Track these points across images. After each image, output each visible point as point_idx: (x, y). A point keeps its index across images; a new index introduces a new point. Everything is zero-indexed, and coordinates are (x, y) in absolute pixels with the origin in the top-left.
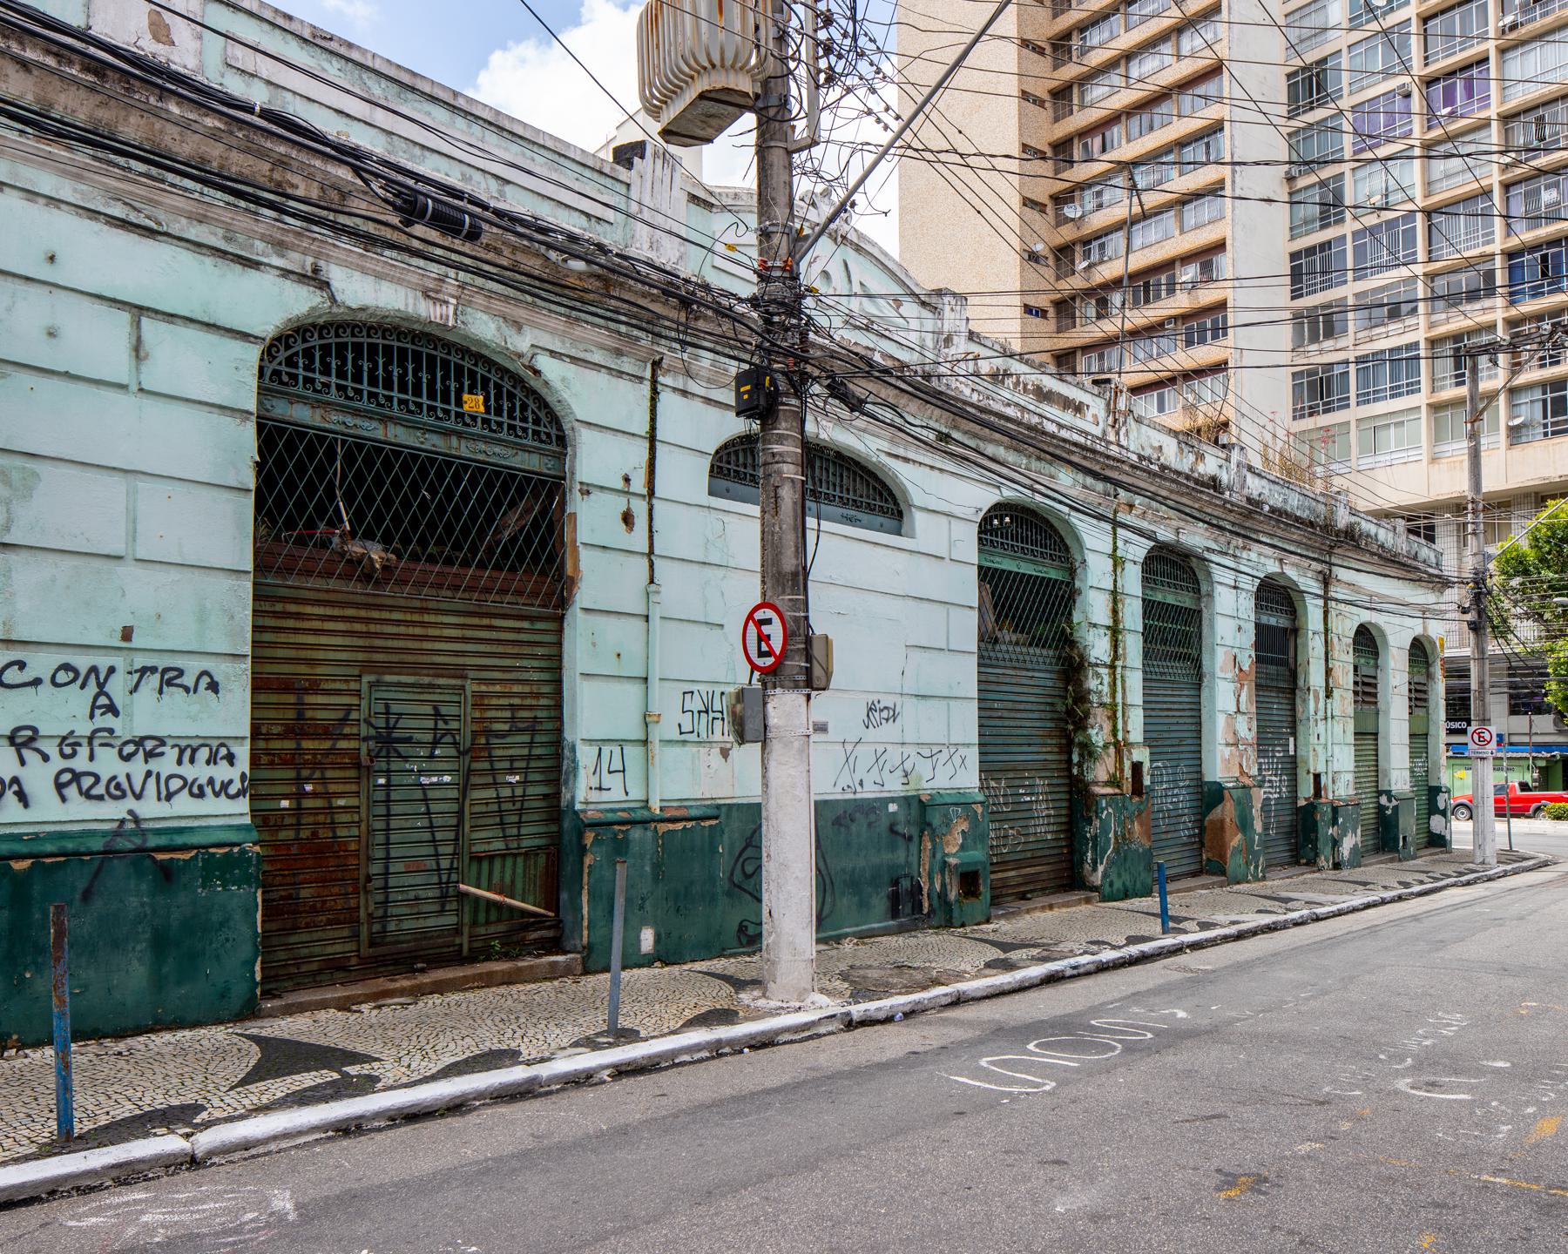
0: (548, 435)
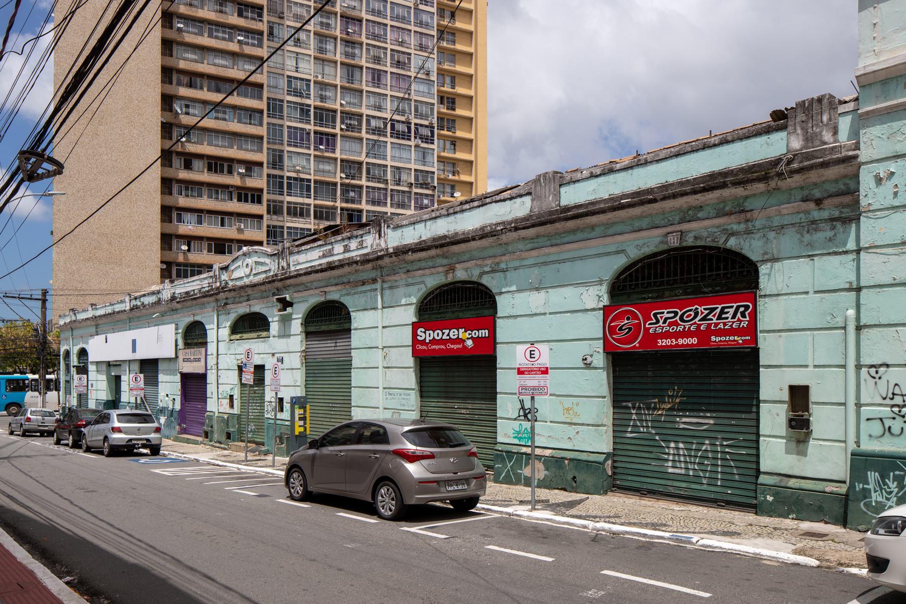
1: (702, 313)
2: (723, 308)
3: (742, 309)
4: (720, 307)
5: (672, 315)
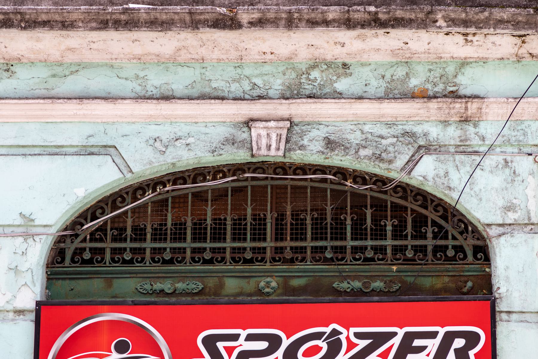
0: (459, 249)
1: (351, 345)
2: (409, 337)
3: (459, 343)
4: (401, 332)
5: (263, 345)
